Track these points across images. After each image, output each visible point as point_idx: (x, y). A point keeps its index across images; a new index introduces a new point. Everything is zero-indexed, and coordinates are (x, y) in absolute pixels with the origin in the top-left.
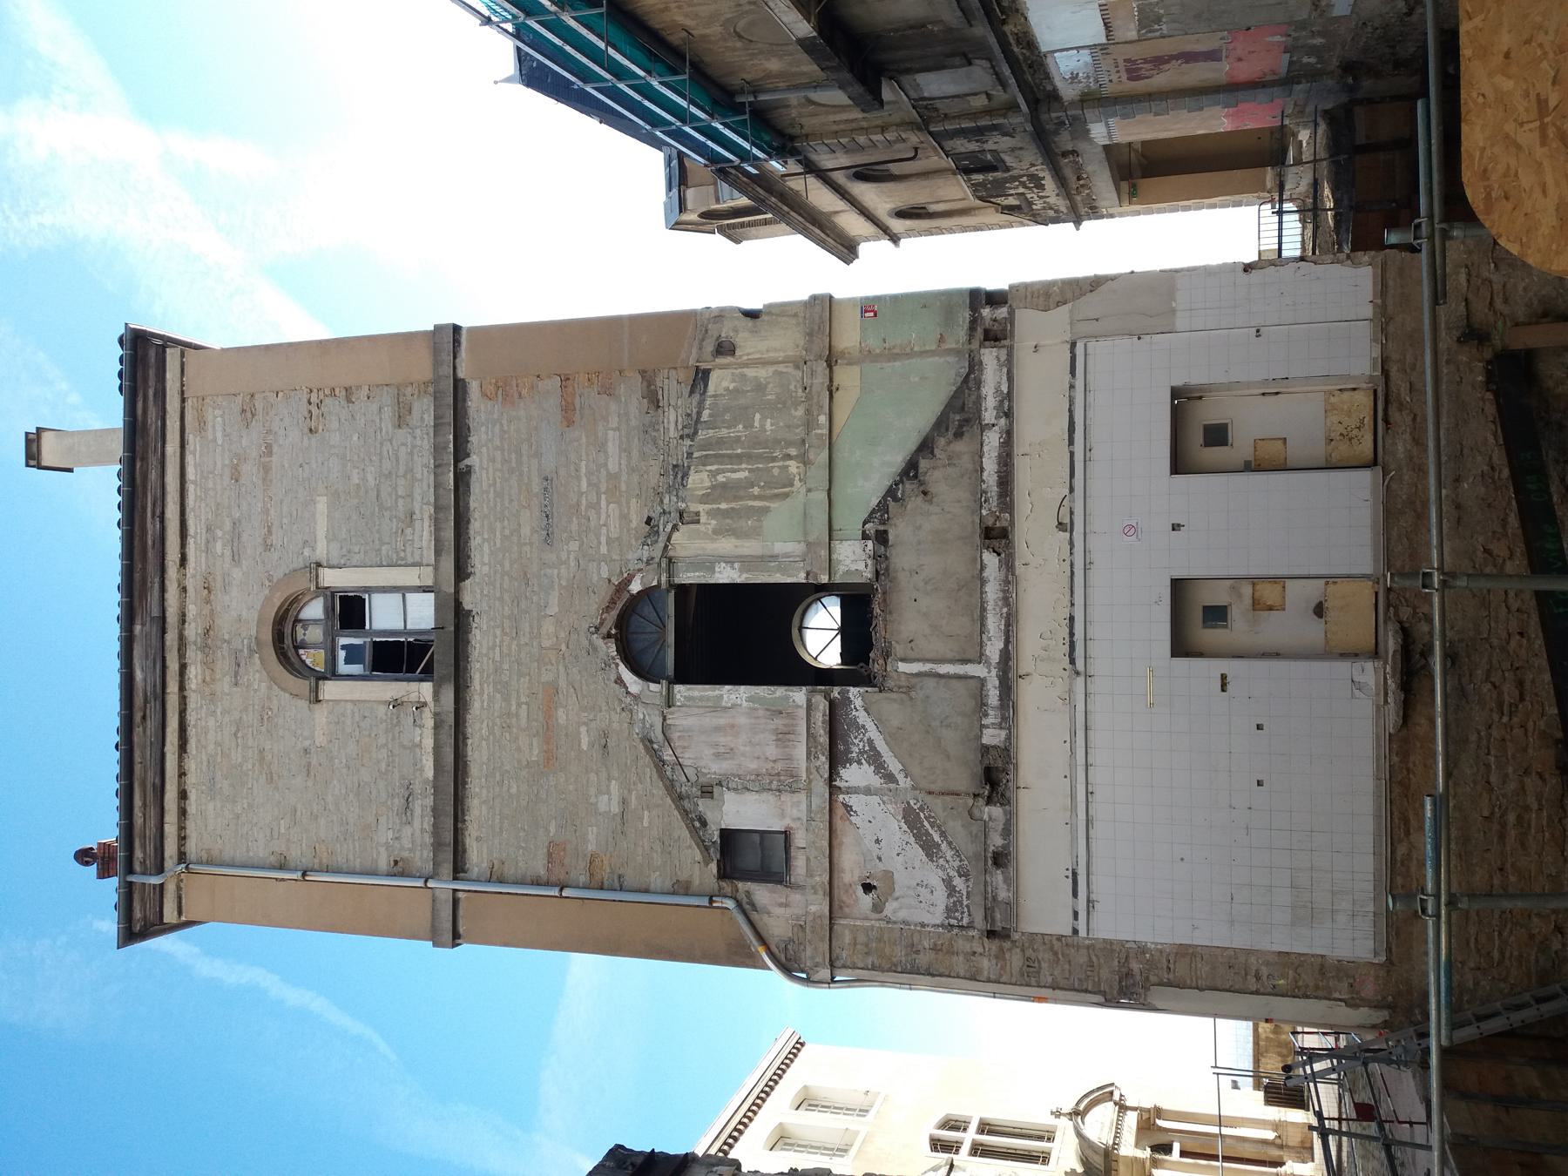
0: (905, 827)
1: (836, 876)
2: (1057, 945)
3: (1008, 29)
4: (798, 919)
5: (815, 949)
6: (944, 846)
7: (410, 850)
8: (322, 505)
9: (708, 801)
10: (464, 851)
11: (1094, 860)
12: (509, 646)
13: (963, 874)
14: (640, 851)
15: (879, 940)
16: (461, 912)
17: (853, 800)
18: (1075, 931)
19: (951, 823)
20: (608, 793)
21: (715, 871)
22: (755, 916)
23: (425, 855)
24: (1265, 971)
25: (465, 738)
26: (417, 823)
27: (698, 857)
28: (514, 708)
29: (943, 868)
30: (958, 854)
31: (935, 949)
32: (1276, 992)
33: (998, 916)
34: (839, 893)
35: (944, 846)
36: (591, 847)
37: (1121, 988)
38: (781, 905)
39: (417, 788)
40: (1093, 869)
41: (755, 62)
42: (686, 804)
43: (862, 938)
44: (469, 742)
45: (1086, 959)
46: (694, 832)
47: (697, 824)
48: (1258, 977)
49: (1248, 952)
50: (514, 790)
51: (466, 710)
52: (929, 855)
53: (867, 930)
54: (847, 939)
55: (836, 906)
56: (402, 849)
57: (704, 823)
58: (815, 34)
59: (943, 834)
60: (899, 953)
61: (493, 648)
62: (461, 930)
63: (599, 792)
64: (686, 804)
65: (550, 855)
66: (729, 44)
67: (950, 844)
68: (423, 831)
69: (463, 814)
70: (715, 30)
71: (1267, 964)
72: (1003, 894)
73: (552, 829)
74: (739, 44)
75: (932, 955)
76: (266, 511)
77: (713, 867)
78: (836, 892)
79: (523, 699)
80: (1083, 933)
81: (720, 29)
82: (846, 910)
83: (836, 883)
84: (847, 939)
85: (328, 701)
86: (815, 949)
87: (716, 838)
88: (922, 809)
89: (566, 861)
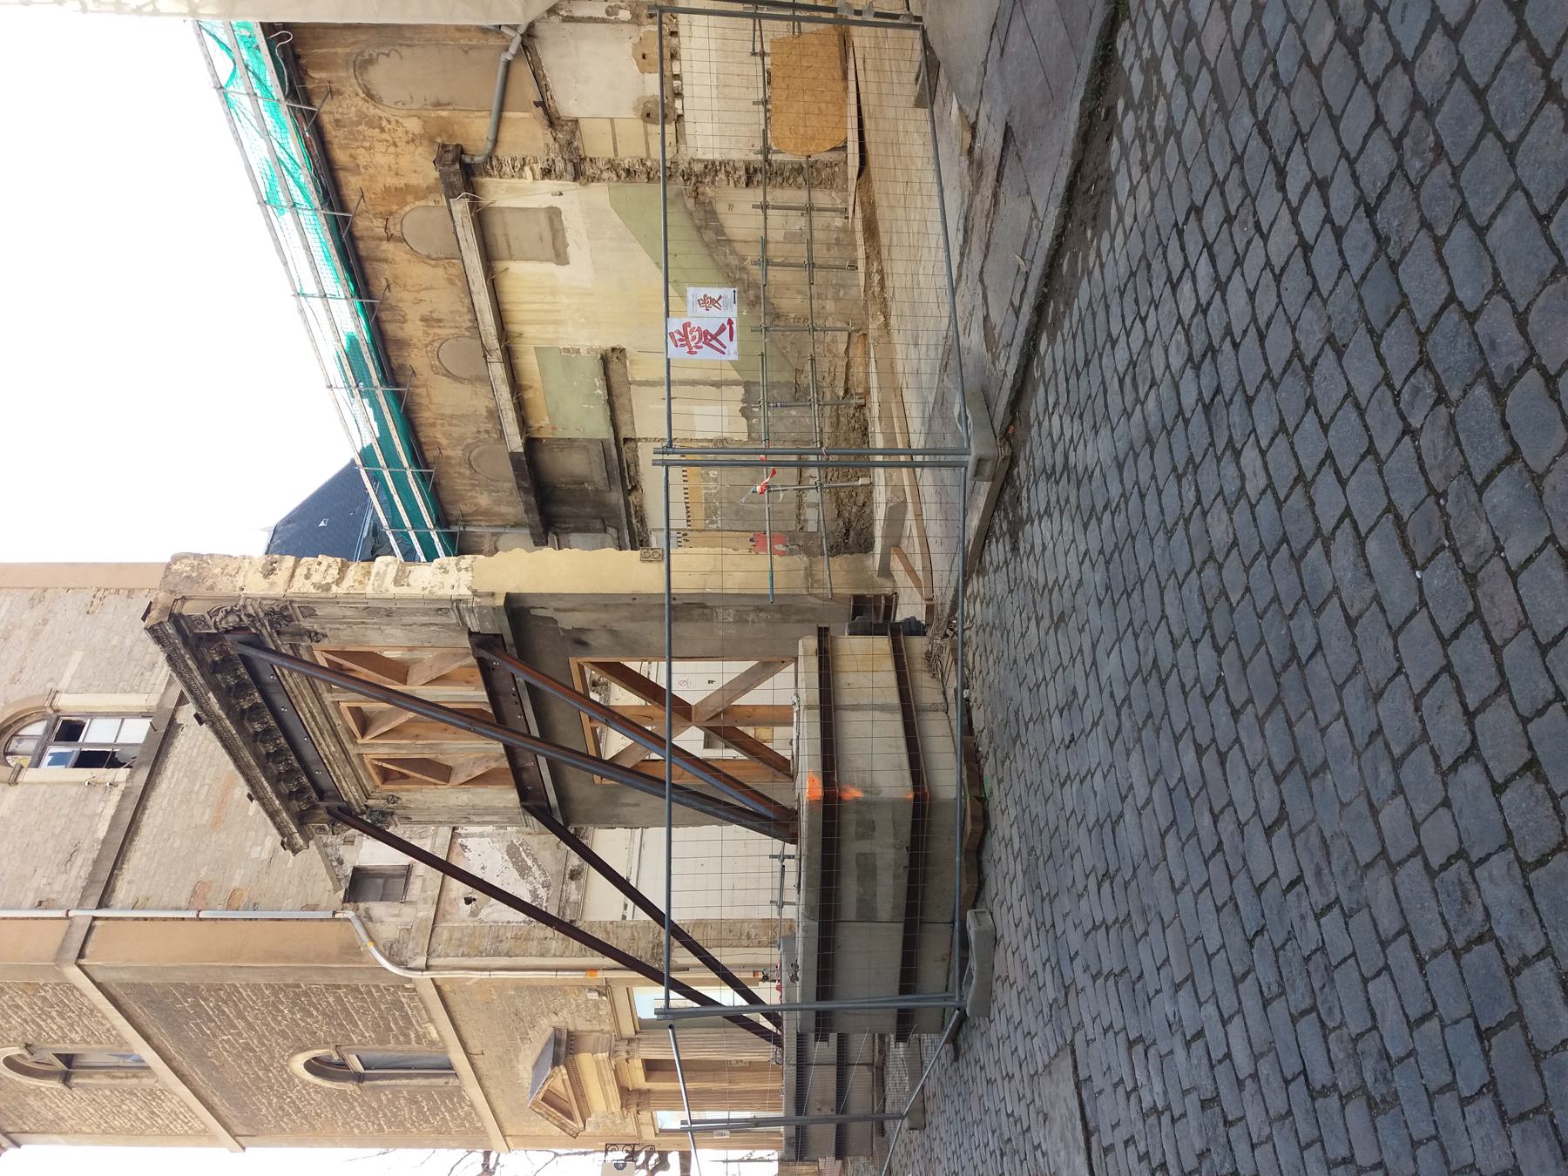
0: (506, 857)
1: (444, 893)
2: (609, 927)
3: (632, 498)
4: (406, 924)
5: (417, 943)
6: (535, 869)
7: (59, 893)
8: (77, 656)
9: (349, 847)
10: (113, 891)
11: (642, 870)
12: (207, 747)
13: (546, 885)
14: (279, 884)
15: (471, 935)
16: (93, 936)
17: (468, 842)
18: (624, 917)
19: (542, 853)
20: (262, 844)
21: (342, 896)
22: (370, 924)
23: (73, 895)
24: (753, 932)
25: (145, 809)
26: (74, 872)
27: (330, 885)
28: (196, 788)
29: (531, 883)
30: (544, 872)
31: (516, 938)
32: (760, 944)
33: (568, 912)
34: (443, 905)
35: (535, 869)
36: (235, 884)
37: (653, 954)
38: (394, 916)
39: (85, 845)
40: (641, 875)
41: (474, 494)
42: (329, 850)
43: (457, 935)
44: (147, 812)
45: (629, 935)
46: (330, 868)
47: (335, 863)
48: (748, 936)
49: (743, 921)
50: (177, 844)
51: (153, 789)
52: (522, 875)
53: (462, 929)
54: (445, 935)
55: (440, 914)
56: (52, 892)
57: (341, 862)
58: (521, 450)
59: (535, 860)
60: (486, 944)
61: (192, 749)
62: (88, 951)
63: (255, 844)
64: (329, 850)
65: (194, 892)
66: (462, 470)
67: (539, 866)
68: (78, 877)
69: (123, 863)
70: (456, 453)
71: (755, 927)
72: (574, 897)
73: (203, 873)
74: (467, 472)
75: (513, 942)
76: (24, 659)
77: (341, 894)
78: (442, 905)
79: (207, 781)
80: (629, 918)
81: (459, 453)
82: (448, 917)
83: (443, 898)
84: (445, 935)
85: (24, 783)
86: (417, 943)
87: (349, 872)
88: (521, 845)
89: (209, 895)
